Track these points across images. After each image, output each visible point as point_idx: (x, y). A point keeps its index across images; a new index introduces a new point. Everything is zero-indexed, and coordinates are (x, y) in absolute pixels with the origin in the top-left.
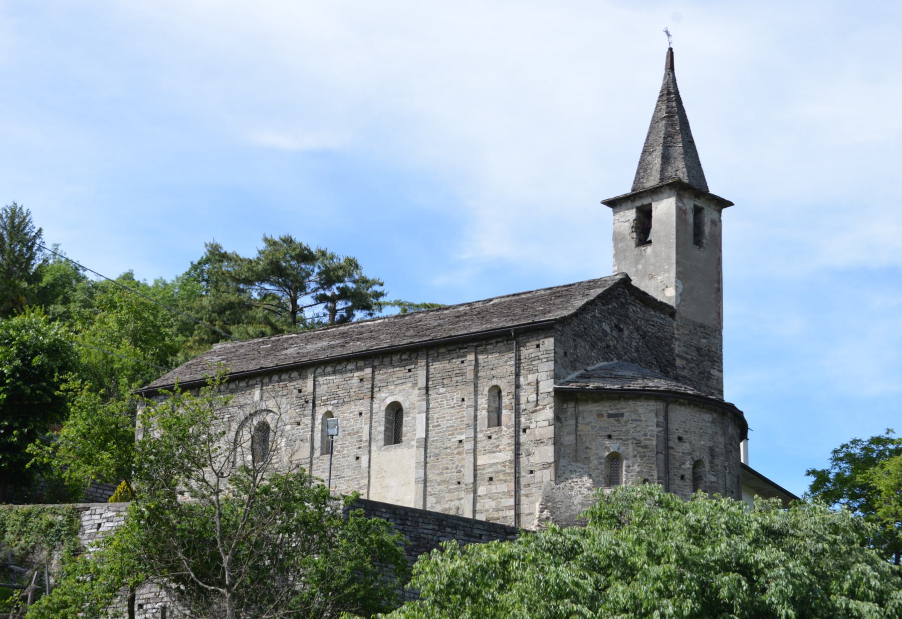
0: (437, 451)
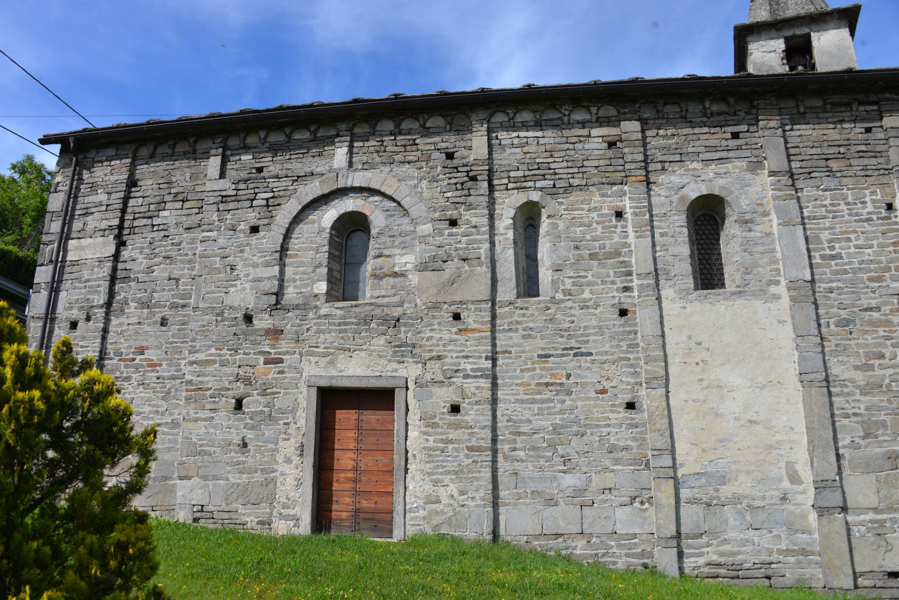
0: (844, 314)
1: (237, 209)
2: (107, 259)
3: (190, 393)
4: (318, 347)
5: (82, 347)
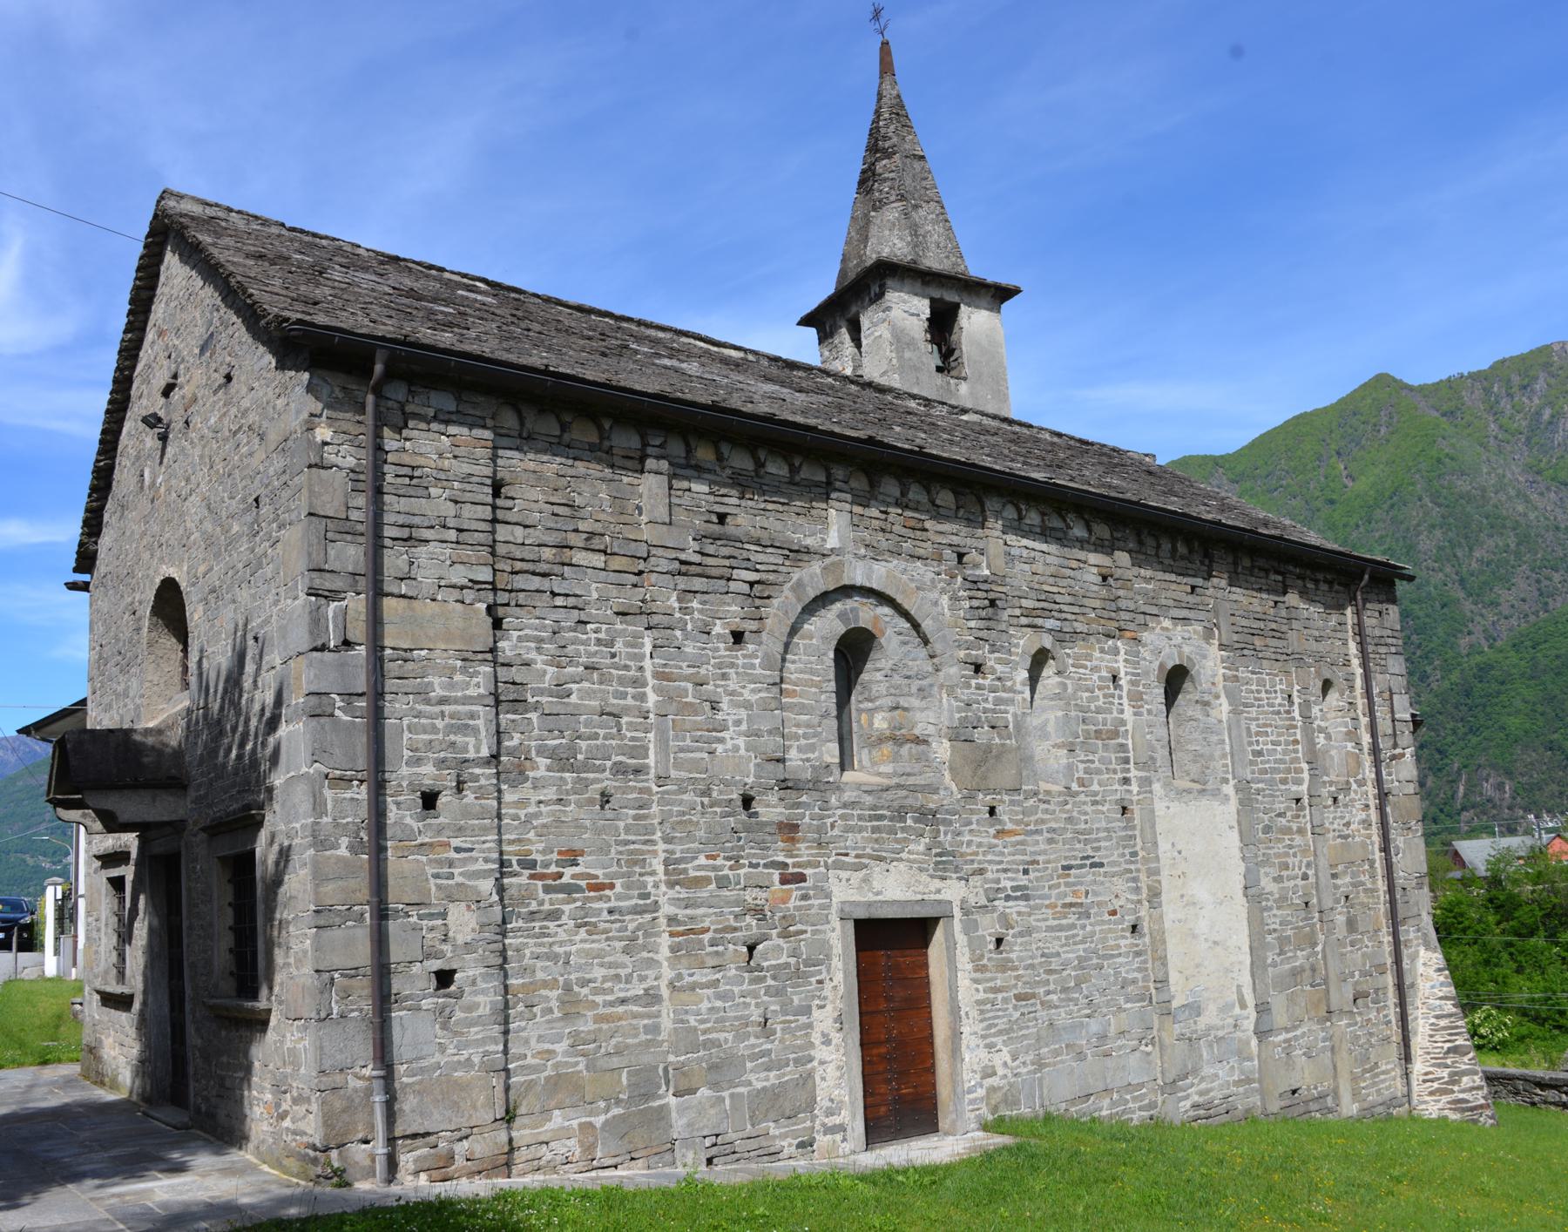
1: (706, 593)
2: (480, 656)
3: (676, 939)
4: (847, 855)
5: (458, 850)
